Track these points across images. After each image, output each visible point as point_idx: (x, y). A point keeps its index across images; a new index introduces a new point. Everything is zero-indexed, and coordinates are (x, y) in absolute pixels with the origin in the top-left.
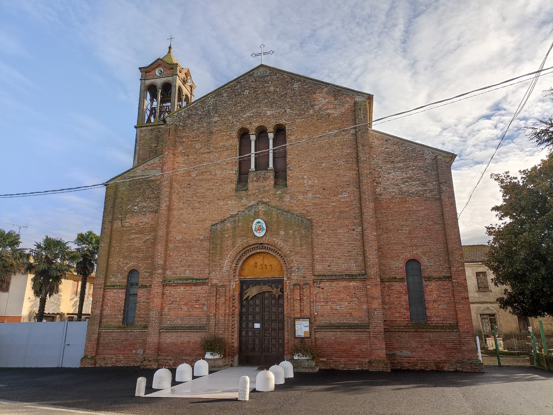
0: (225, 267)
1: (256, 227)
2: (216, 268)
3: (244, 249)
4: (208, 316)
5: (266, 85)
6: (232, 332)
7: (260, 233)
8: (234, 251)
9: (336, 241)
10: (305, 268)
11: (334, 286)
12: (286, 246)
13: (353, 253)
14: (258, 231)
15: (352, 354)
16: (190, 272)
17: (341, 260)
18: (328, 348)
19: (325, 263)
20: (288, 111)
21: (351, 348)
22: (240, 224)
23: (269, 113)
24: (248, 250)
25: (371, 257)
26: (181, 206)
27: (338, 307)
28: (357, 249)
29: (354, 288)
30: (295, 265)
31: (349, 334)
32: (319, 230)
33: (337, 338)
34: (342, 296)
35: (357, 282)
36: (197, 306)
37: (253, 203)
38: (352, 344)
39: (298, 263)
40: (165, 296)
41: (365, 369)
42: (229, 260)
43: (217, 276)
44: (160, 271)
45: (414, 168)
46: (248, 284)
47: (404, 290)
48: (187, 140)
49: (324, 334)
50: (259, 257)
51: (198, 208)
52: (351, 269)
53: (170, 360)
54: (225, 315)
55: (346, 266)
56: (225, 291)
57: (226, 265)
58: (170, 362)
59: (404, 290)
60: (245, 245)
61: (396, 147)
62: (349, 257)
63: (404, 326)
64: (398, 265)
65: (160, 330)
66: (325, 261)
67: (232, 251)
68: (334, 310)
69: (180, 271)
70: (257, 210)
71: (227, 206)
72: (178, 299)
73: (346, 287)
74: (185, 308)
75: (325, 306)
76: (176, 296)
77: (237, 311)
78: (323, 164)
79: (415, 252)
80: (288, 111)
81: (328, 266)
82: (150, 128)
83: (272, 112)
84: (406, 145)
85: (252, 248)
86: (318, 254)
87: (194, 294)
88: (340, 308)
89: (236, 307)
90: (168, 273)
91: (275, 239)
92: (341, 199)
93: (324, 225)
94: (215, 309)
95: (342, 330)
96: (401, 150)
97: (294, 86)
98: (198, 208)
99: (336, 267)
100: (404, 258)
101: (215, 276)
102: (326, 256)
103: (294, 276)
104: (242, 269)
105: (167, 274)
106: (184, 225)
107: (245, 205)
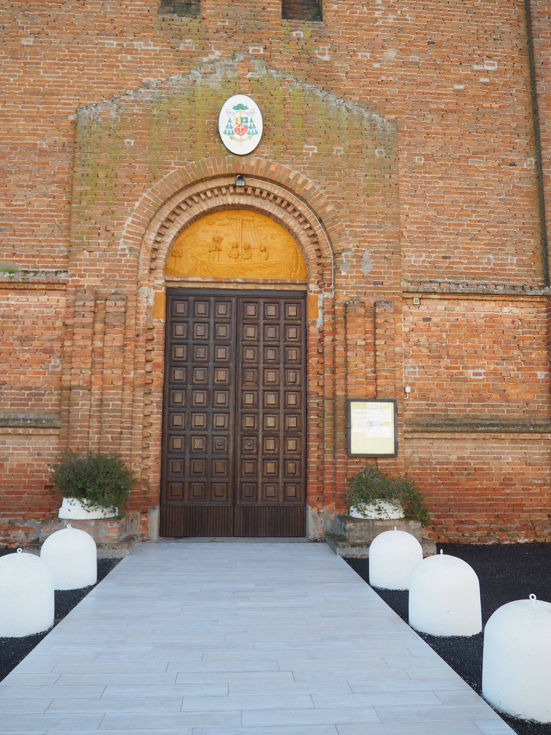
0: (125, 237)
1: (230, 121)
2: (92, 238)
3: (186, 187)
4: (62, 388)
6: (145, 437)
7: (241, 141)
8: (153, 190)
9: (466, 189)
11: (458, 315)
12: (321, 188)
14: (236, 136)
15: (504, 500)
18: (439, 485)
19: (435, 247)
21: (501, 484)
24: (198, 195)
29: (513, 322)
30: (351, 246)
31: (498, 448)
32: (417, 155)
33: (463, 458)
35: (522, 305)
36: (27, 355)
38: (504, 474)
39: (360, 242)
41: (541, 540)
43: (95, 265)
46: (192, 298)
49: (429, 448)
50: (227, 221)
52: (506, 270)
54: (124, 384)
55: (493, 261)
56: (123, 309)
57: (128, 232)
60: (192, 176)
62: (501, 236)
66: (434, 243)
67: (149, 190)
68: (457, 380)
71: (129, 58)
73: (492, 317)
77: (158, 375)
81: (444, 258)
85: (212, 190)
86: (415, 223)
88: (475, 374)
91: (287, 166)
92: (480, 76)
93: (433, 141)
94: (89, 366)
95: (482, 435)
99: (466, 261)
101: (90, 265)
102: (438, 230)
103: (346, 277)
104: (173, 253)
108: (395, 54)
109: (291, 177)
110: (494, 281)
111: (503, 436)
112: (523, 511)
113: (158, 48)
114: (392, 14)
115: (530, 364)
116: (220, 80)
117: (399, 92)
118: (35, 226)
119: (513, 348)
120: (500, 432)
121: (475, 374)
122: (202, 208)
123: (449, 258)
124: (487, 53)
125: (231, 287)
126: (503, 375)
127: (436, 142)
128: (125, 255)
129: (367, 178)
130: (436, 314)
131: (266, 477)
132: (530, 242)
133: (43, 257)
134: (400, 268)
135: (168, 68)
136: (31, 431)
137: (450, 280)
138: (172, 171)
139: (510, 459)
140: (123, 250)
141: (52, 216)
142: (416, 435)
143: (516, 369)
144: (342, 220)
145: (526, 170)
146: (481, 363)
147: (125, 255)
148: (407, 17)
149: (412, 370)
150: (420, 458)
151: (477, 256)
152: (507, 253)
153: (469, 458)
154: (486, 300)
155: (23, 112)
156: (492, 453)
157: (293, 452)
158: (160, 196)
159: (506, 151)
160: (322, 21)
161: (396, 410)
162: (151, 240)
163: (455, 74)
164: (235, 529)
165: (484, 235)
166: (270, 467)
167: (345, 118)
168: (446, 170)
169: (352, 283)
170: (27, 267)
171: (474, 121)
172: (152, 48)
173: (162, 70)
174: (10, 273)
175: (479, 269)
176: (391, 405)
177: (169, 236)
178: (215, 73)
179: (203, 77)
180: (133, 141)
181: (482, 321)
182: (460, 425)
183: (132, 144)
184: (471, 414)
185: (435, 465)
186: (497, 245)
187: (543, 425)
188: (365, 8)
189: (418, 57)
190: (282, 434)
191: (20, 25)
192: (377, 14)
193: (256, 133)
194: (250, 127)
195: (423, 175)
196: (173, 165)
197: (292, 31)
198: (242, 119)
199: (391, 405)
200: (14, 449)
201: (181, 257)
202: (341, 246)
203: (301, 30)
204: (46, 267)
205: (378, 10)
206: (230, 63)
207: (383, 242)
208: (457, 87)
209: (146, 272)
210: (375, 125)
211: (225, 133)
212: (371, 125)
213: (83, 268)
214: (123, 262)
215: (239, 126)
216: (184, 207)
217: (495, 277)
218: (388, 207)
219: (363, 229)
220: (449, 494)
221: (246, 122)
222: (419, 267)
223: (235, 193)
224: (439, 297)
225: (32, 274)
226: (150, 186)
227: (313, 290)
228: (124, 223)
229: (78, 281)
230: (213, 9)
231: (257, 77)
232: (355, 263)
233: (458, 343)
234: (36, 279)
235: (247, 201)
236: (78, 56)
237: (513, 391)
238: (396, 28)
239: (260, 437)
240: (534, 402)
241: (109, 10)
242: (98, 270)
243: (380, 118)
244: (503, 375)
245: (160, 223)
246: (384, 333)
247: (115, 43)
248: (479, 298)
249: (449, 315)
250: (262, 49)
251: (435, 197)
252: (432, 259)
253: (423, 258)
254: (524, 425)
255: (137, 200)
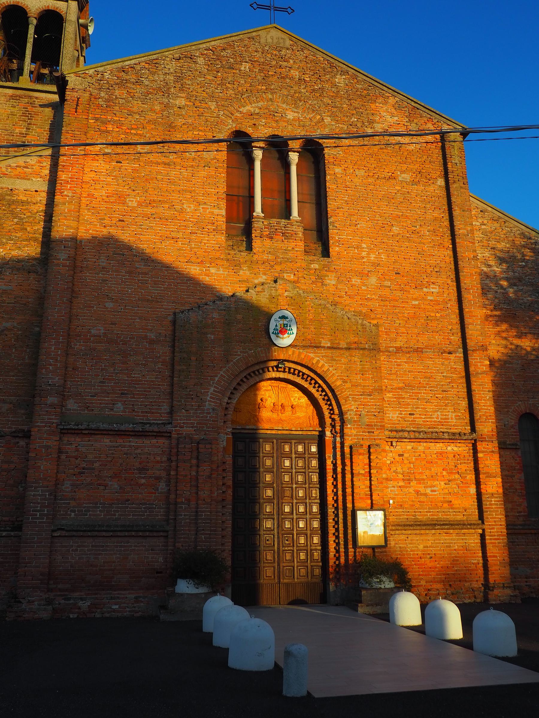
0: (209, 401)
1: (276, 326)
5: (285, 64)
8: (227, 370)
9: (422, 369)
10: (371, 415)
11: (420, 452)
12: (333, 370)
13: (450, 394)
15: (454, 574)
16: (124, 408)
17: (431, 406)
20: (327, 120)
22: (239, 317)
23: (290, 116)
24: (254, 372)
25: (483, 403)
26: (103, 262)
27: (428, 491)
28: (457, 388)
29: (454, 456)
30: (353, 407)
31: (449, 539)
33: (427, 547)
34: (435, 469)
36: (143, 481)
37: (262, 278)
38: (453, 557)
40: (63, 457)
42: (218, 388)
44: (51, 400)
45: (523, 263)
47: (518, 463)
48: (118, 130)
51: (142, 273)
52: (448, 422)
53: (82, 599)
55: (440, 417)
58: (80, 603)
59: (518, 463)
61: (497, 225)
63: (521, 525)
64: (508, 422)
65: (53, 531)
66: (404, 405)
68: (421, 494)
69: (100, 404)
70: (273, 293)
72: (96, 465)
74: (115, 485)
75: (406, 487)
76: (90, 457)
78: (394, 228)
79: (531, 402)
80: (327, 120)
81: (410, 414)
82: (10, 92)
83: (296, 114)
84: (511, 226)
87: (136, 454)
88: (432, 491)
89: (229, 487)
90: (71, 405)
96: (504, 232)
97: (337, 80)
98: (142, 273)
99: (423, 417)
100: (516, 410)
101: (187, 420)
102: (406, 396)
103: (351, 428)
104: (236, 410)
105: (69, 407)
106: (110, 305)
107: (247, 281)
108: (375, 280)
109: (314, 362)
110: (441, 430)
111: (451, 531)
112: (466, 581)
113: (226, 273)
114: (373, 254)
115: (466, 483)
116: (268, 297)
117: (379, 305)
118: (147, 391)
119: (455, 473)
120: (449, 529)
121: (432, 491)
122: (256, 380)
123: (413, 414)
124: (432, 281)
125: (274, 432)
126: (450, 491)
127: (402, 339)
128: (209, 413)
129: (361, 363)
130: (406, 452)
131: (299, 562)
132: (462, 404)
133: (153, 413)
134: (384, 422)
135: (233, 286)
136: (147, 534)
137: (414, 429)
138: (239, 357)
139: (456, 546)
140: (208, 409)
141: (159, 385)
142: (397, 532)
143: (457, 487)
144: (347, 390)
145: (458, 357)
146: (435, 483)
147: (209, 413)
148: (382, 257)
149: (393, 488)
150: (400, 547)
151: (430, 413)
152: (449, 411)
153: (431, 547)
154: (437, 442)
155: (138, 313)
156: (445, 543)
157: (316, 545)
158: (231, 374)
159: (445, 344)
160: (330, 257)
161: (385, 515)
162: (225, 402)
163: (412, 294)
164: (281, 599)
165: (434, 400)
166: (302, 556)
167: (346, 324)
168: (409, 357)
169: (355, 432)
170: (143, 419)
171: (425, 325)
172: (221, 272)
173: (229, 287)
174: (133, 424)
175: (431, 422)
176: (382, 512)
177: (235, 399)
178: (264, 291)
179: (257, 295)
180: (213, 336)
181: (435, 456)
182: (425, 525)
183: (213, 339)
184: (431, 517)
185: (410, 552)
186: (442, 406)
187: (476, 524)
188: (356, 250)
189: (389, 283)
190: (309, 532)
191: (135, 254)
192: (364, 254)
193: (293, 333)
194: (289, 330)
195: (395, 360)
196: (239, 353)
197: (311, 264)
198: (284, 324)
199: (382, 512)
200: (135, 546)
201: (240, 411)
202: (346, 408)
203: (316, 263)
204: (155, 420)
205: (364, 251)
206: (273, 286)
207: (373, 405)
208: (414, 303)
209: (222, 424)
210: (365, 328)
211: (273, 333)
212: (363, 328)
213: (182, 422)
214: (208, 418)
215: (282, 329)
216: (245, 380)
217: (442, 427)
218: (375, 382)
219: (360, 397)
220: (419, 571)
221: (287, 326)
222: (395, 420)
223: (277, 371)
224: (409, 441)
225: (148, 425)
226: (225, 367)
227: (328, 435)
228: (209, 392)
229: (180, 431)
230: (261, 248)
231: (291, 295)
232: (356, 419)
233: (421, 471)
234: (151, 429)
235: (285, 376)
236: (174, 277)
237: (456, 502)
238: (375, 263)
239: (295, 535)
240: (469, 508)
241: (193, 246)
242: (192, 423)
243: (368, 324)
244: (450, 491)
245: (230, 391)
246: (376, 465)
247: (198, 268)
248: (433, 441)
249: (414, 452)
250: (292, 275)
251: (403, 374)
252: (403, 416)
253: (397, 415)
254: (464, 525)
255: (217, 376)
